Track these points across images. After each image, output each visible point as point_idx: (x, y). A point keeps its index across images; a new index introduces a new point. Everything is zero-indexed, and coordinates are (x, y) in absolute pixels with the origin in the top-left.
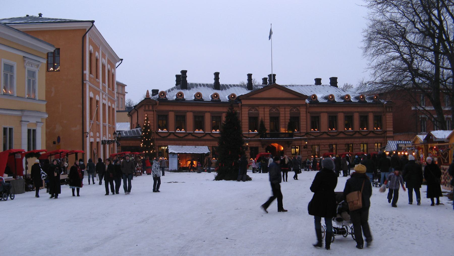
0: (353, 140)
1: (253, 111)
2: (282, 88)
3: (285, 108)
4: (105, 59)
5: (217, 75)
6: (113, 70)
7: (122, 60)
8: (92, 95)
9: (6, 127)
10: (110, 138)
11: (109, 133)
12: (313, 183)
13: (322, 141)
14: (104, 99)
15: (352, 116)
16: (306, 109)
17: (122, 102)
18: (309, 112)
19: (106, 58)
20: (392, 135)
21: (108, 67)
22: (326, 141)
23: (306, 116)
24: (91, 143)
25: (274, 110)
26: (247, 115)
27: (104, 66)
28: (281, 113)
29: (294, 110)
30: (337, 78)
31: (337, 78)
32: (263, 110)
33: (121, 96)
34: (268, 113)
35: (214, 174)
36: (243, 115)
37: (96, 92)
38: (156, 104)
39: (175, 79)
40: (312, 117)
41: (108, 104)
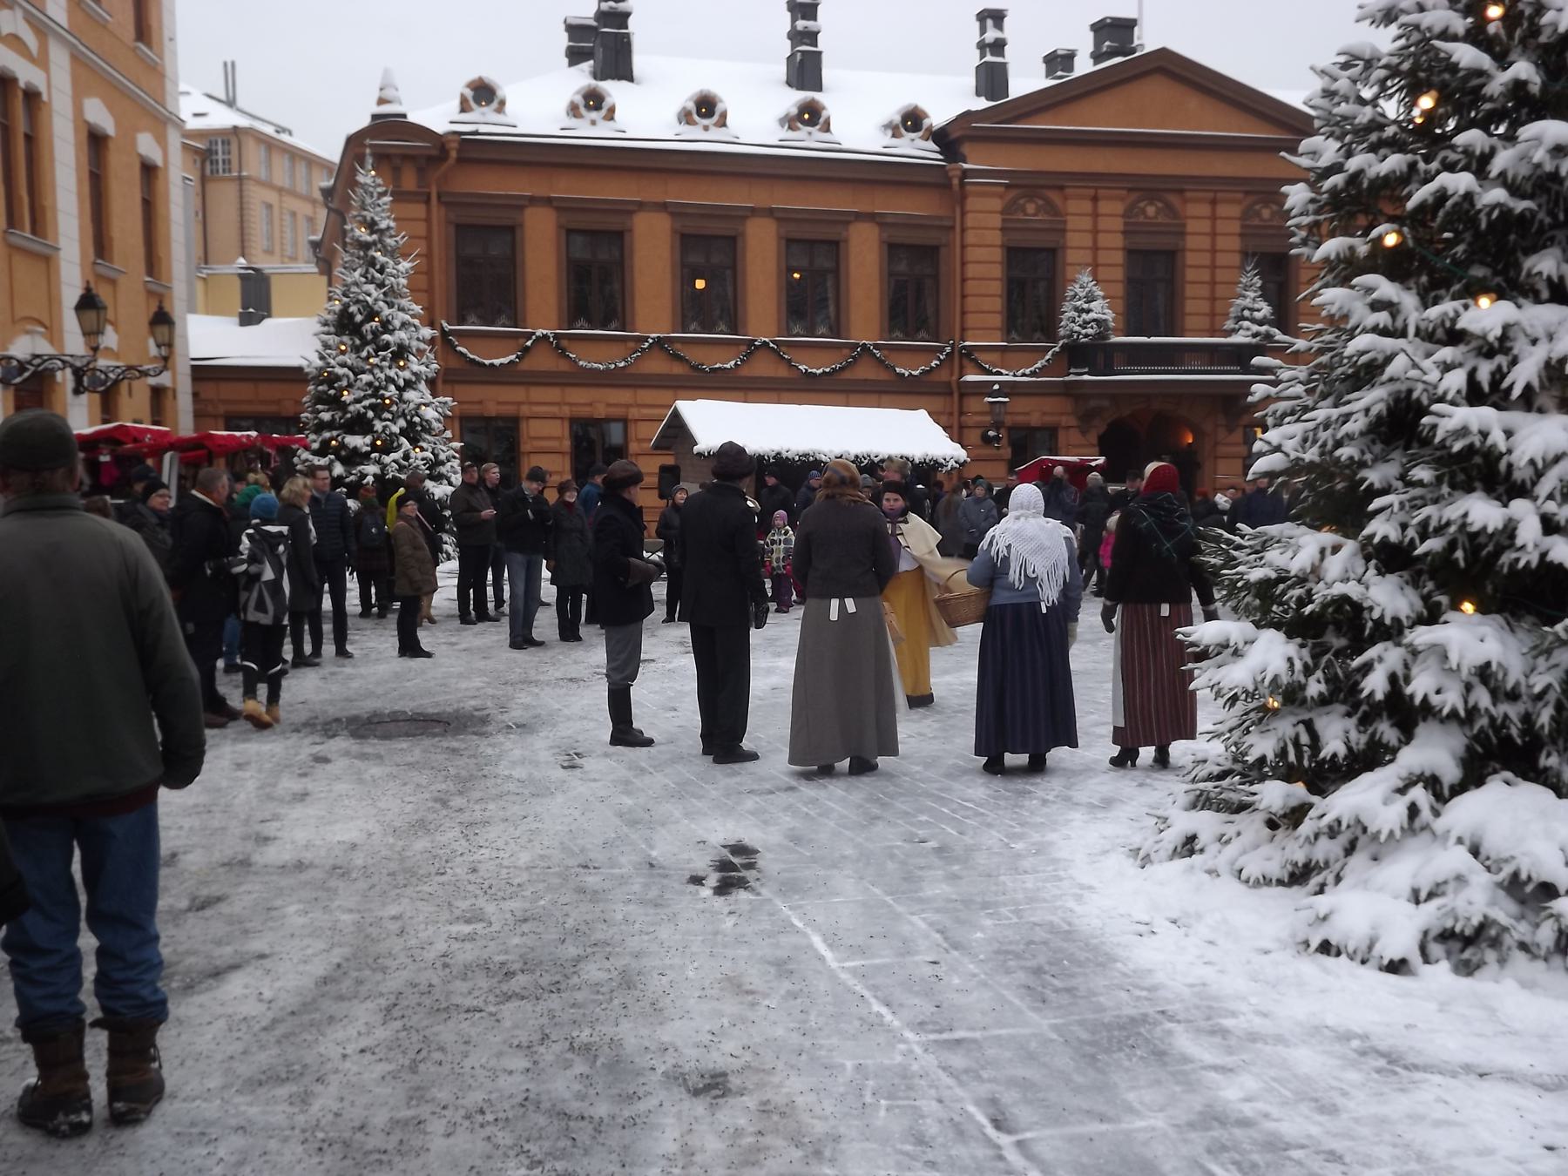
0: (623, 396)
2: (1169, 66)
3: (1095, 199)
12: (201, 762)
13: (538, 393)
22: (553, 394)
25: (1151, 210)
28: (1191, 226)
29: (1151, 210)
32: (1087, 206)
34: (1118, 224)
35: (1121, 724)
36: (971, 237)
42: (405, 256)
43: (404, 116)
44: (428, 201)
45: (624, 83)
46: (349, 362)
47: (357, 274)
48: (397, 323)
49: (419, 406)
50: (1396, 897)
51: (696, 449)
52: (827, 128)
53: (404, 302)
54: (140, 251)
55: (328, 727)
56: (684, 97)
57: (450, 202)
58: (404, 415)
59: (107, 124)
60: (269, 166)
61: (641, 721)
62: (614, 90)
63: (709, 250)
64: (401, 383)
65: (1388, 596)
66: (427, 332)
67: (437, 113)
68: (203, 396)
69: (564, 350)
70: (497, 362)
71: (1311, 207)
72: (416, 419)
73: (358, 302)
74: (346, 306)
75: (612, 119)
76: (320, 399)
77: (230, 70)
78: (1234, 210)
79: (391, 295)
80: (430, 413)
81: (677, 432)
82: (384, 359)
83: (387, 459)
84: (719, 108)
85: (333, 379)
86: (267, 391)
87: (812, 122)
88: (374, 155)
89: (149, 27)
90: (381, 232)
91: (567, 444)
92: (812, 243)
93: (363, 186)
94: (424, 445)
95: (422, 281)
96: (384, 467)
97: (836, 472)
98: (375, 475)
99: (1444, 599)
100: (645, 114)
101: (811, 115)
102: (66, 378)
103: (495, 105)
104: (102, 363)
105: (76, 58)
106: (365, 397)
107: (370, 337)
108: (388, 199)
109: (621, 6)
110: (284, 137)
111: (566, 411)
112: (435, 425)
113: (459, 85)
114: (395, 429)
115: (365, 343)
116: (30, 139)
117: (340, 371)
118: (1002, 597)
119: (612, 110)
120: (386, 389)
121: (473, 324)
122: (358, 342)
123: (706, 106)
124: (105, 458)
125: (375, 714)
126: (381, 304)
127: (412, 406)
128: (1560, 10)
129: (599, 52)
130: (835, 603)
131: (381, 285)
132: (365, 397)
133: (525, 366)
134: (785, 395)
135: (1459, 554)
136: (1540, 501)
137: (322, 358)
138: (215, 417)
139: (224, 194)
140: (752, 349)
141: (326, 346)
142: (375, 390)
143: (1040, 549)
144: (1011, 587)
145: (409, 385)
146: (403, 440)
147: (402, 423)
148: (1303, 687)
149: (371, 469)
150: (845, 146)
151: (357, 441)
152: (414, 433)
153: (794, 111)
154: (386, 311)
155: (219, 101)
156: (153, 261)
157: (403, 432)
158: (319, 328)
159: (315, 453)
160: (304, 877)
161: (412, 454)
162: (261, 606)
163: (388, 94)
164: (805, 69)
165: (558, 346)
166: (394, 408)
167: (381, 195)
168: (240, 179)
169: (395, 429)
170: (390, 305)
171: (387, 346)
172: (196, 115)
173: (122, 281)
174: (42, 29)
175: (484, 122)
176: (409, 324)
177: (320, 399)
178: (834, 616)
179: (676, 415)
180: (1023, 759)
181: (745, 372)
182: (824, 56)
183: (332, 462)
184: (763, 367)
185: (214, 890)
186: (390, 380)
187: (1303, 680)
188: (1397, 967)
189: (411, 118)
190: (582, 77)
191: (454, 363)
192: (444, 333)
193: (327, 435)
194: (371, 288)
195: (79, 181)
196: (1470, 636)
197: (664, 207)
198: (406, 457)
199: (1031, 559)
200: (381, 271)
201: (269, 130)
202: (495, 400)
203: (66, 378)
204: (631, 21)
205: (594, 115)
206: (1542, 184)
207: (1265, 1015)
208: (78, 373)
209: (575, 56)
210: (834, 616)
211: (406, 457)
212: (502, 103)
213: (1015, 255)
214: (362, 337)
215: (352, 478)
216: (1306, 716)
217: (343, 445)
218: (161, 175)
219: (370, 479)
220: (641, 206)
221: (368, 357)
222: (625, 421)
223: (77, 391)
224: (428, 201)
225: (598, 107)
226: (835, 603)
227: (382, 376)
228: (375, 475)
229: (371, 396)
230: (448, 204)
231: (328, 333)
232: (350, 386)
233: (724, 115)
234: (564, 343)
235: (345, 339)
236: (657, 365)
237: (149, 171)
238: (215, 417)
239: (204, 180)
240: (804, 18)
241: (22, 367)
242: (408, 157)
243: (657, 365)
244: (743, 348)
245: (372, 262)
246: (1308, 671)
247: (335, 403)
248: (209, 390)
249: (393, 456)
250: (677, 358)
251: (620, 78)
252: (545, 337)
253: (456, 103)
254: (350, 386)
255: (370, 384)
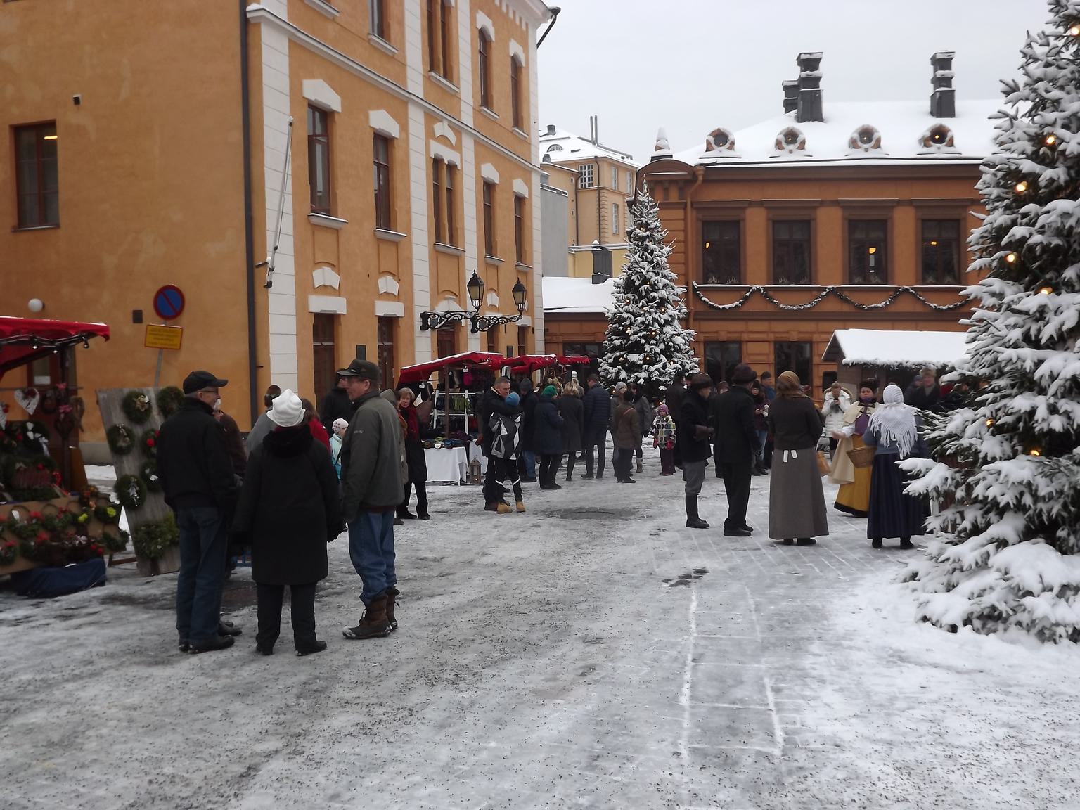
7: (556, 11)
13: (754, 326)
14: (443, 140)
42: (667, 242)
43: (671, 156)
44: (685, 208)
45: (816, 123)
46: (631, 310)
47: (637, 256)
48: (660, 285)
49: (672, 336)
50: (963, 596)
51: (844, 361)
52: (951, 144)
53: (666, 272)
54: (514, 248)
55: (549, 513)
56: (851, 131)
57: (699, 207)
58: (664, 341)
59: (495, 177)
60: (617, 180)
61: (702, 513)
62: (807, 130)
63: (867, 231)
64: (662, 322)
65: (990, 446)
66: (679, 290)
67: (691, 153)
68: (550, 331)
69: (770, 298)
70: (727, 306)
71: (981, 241)
72: (671, 344)
73: (637, 273)
74: (630, 276)
75: (803, 148)
76: (615, 332)
77: (594, 121)
79: (657, 267)
80: (679, 340)
81: (836, 351)
82: (651, 307)
83: (652, 369)
84: (876, 136)
85: (620, 320)
86: (590, 327)
87: (941, 141)
88: (648, 182)
89: (522, 118)
90: (652, 230)
91: (772, 358)
92: (940, 221)
93: (641, 202)
94: (676, 360)
95: (681, 257)
96: (650, 373)
97: (782, 383)
98: (644, 378)
99: (1019, 448)
100: (826, 144)
101: (939, 136)
102: (467, 324)
103: (728, 145)
104: (488, 314)
105: (477, 143)
106: (640, 331)
107: (644, 294)
108: (656, 209)
109: (815, 73)
110: (627, 161)
111: (772, 337)
112: (683, 347)
113: (705, 135)
114: (658, 350)
115: (641, 298)
116: (450, 191)
117: (626, 315)
118: (879, 452)
119: (803, 143)
120: (652, 326)
121: (713, 283)
122: (637, 297)
123: (867, 136)
124: (465, 370)
125: (581, 509)
126: (651, 273)
127: (668, 336)
128: (1068, 143)
129: (800, 103)
130: (786, 452)
131: (651, 262)
132: (640, 331)
133: (746, 308)
134: (921, 324)
135: (1021, 425)
136: (1048, 396)
137: (616, 308)
138: (557, 343)
139: (589, 200)
140: (897, 294)
141: (618, 300)
142: (646, 326)
143: (898, 424)
144: (882, 446)
145: (667, 323)
146: (662, 357)
147: (662, 346)
148: (954, 493)
149: (643, 375)
150: (964, 155)
151: (634, 358)
152: (669, 353)
153: (928, 134)
154: (654, 278)
155: (588, 141)
156: (521, 253)
157: (662, 352)
158: (614, 289)
159: (610, 365)
160: (494, 568)
161: (668, 365)
162: (498, 448)
163: (661, 143)
164: (943, 104)
165: (767, 295)
166: (657, 337)
167: (654, 207)
168: (599, 189)
169: (658, 350)
170: (657, 274)
171: (654, 298)
172: (572, 151)
173: (503, 267)
174: (458, 131)
175: (721, 157)
176: (670, 286)
177: (615, 332)
178: (785, 460)
179: (835, 339)
180: (896, 541)
181: (893, 309)
182: (957, 95)
183: (619, 370)
184: (905, 306)
185: (452, 571)
186: (655, 320)
187: (954, 489)
188: (953, 629)
189: (675, 158)
190: (788, 121)
191: (701, 308)
192: (695, 290)
193: (617, 354)
194: (645, 264)
195: (478, 211)
196: (1021, 469)
197: (837, 203)
198: (664, 367)
199: (892, 431)
200: (651, 254)
201: (618, 157)
202: (724, 331)
203: (467, 324)
204: (821, 83)
205: (791, 147)
206: (1065, 233)
207: (685, 580)
208: (474, 320)
209: (789, 106)
210: (785, 460)
211: (664, 367)
212: (733, 143)
214: (640, 295)
215: (631, 380)
216: (961, 509)
217: (626, 360)
218: (527, 202)
219: (642, 381)
220: (822, 203)
221: (643, 306)
222: (811, 343)
223: (473, 331)
224: (685, 208)
225: (794, 142)
226: (786, 452)
227: (651, 318)
228: (644, 378)
229: (643, 330)
230: (698, 209)
231: (620, 293)
232: (631, 324)
233: (879, 141)
234: (771, 293)
235: (630, 295)
236: (832, 306)
237: (520, 200)
238: (557, 343)
239: (577, 191)
240: (942, 69)
241: (442, 317)
242: (673, 182)
243: (832, 306)
244: (892, 293)
245: (646, 249)
246: (958, 485)
247: (622, 334)
248: (554, 328)
249: (656, 366)
250: (846, 301)
251: (814, 120)
252: (758, 290)
253: (704, 146)
254: (631, 324)
255: (643, 323)
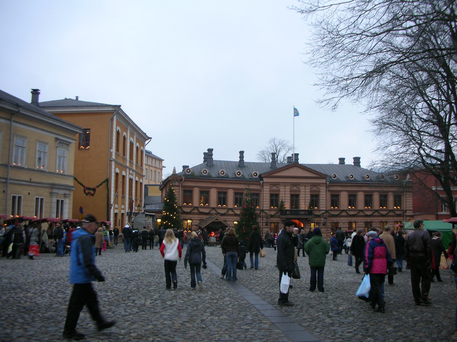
1: (315, 189)
2: (304, 167)
4: (133, 138)
5: (242, 153)
6: (142, 148)
7: (151, 138)
8: (118, 170)
9: (58, 199)
10: (136, 210)
11: (136, 206)
15: (258, 195)
16: (327, 187)
17: (159, 176)
18: (329, 191)
19: (135, 137)
20: (412, 214)
21: (136, 144)
22: (377, 218)
23: (326, 195)
24: (116, 214)
26: (269, 192)
27: (132, 144)
30: (360, 158)
31: (360, 158)
33: (158, 171)
37: (123, 167)
38: (182, 180)
39: (203, 156)
40: (332, 196)
41: (135, 178)
78: (289, 188)
213: (271, 195)
